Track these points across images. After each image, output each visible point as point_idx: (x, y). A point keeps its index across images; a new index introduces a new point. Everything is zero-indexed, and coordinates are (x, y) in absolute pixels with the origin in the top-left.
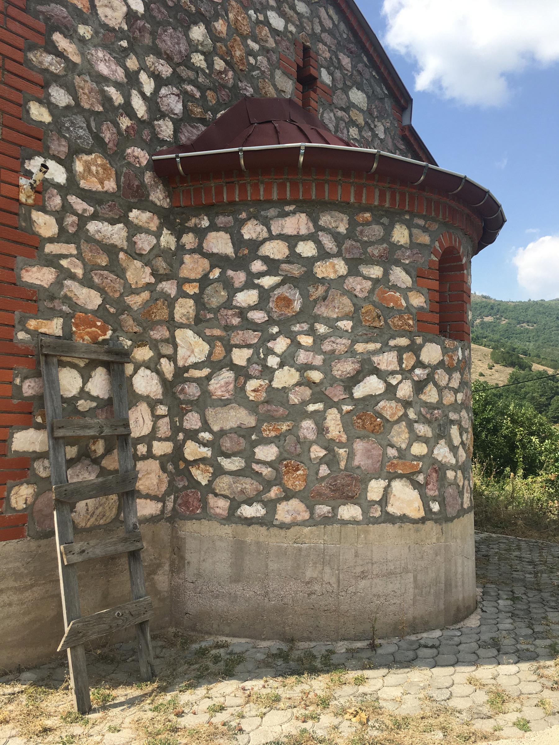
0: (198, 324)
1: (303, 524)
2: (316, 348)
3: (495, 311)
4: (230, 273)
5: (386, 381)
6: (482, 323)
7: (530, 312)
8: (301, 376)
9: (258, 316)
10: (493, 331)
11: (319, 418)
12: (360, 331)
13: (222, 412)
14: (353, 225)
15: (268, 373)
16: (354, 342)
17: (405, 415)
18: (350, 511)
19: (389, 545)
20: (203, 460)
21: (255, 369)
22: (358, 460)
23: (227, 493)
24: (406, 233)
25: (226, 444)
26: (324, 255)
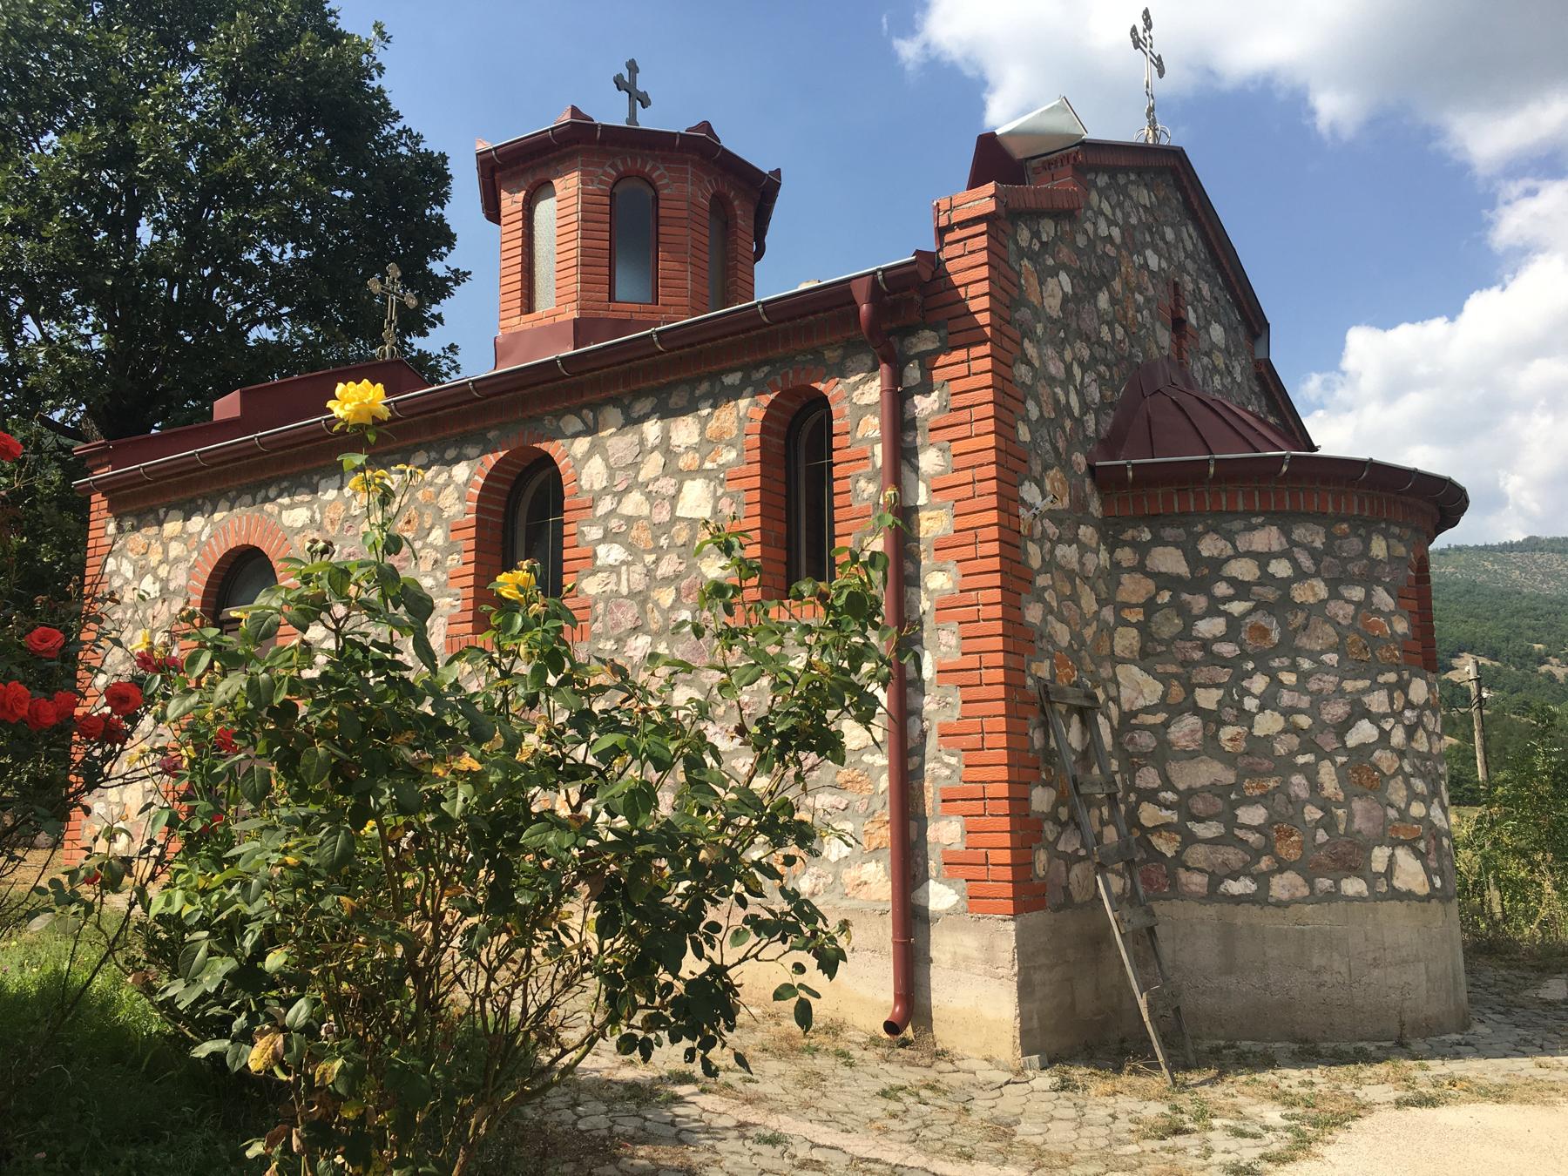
0: (1144, 658)
1: (1304, 901)
2: (1300, 688)
4: (1185, 596)
5: (1379, 727)
8: (1287, 721)
9: (1228, 649)
11: (1310, 772)
12: (1348, 666)
13: (1188, 767)
14: (1330, 537)
15: (1246, 718)
16: (1343, 679)
17: (1401, 767)
18: (1353, 886)
19: (1399, 927)
20: (1167, 826)
21: (1229, 714)
22: (1358, 823)
23: (1203, 865)
24: (1384, 544)
25: (1198, 806)
26: (1300, 575)
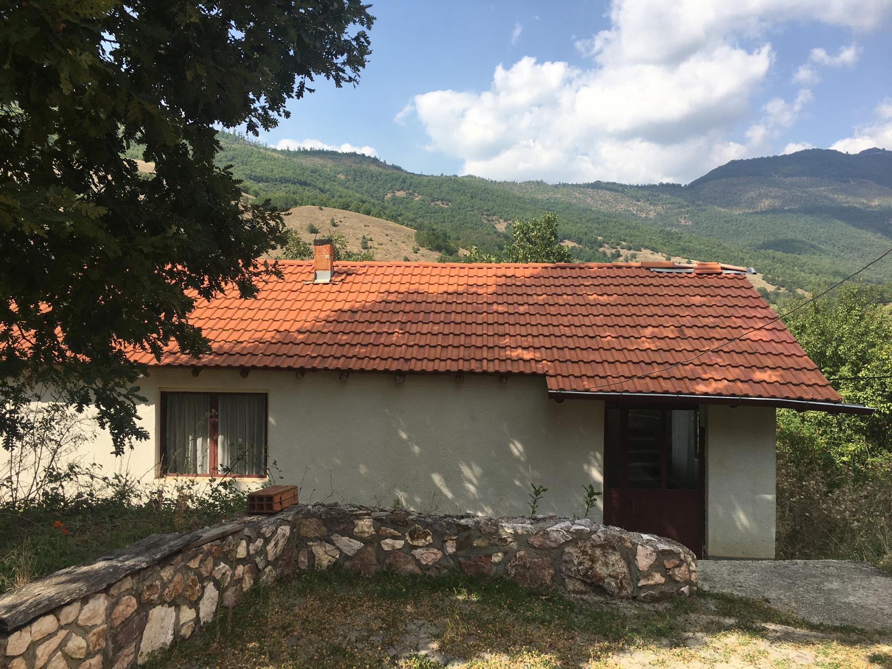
3: (407, 185)
6: (394, 199)
7: (444, 189)
10: (406, 208)
